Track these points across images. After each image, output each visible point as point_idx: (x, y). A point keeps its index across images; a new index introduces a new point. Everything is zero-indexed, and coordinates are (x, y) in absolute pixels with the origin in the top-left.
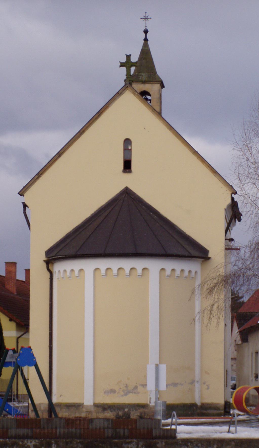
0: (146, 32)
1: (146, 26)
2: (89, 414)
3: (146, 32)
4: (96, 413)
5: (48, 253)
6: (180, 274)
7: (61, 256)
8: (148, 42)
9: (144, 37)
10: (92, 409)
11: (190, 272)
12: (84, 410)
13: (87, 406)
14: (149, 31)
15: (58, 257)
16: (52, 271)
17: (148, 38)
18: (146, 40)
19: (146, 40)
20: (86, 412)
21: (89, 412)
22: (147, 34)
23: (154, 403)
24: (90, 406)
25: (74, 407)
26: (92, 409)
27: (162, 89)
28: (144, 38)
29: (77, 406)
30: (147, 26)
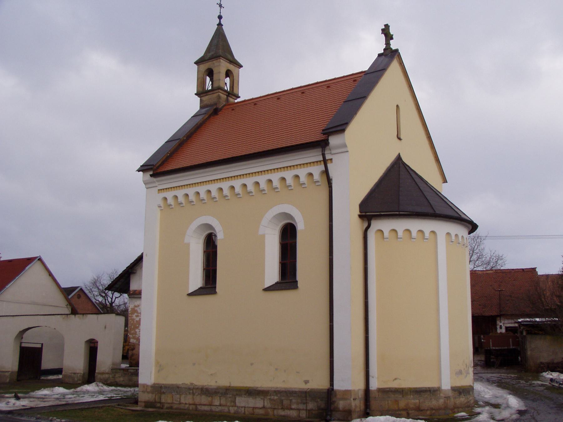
0: (220, 17)
1: (220, 13)
2: (447, 401)
3: (220, 17)
4: (454, 398)
5: (363, 205)
6: (402, 235)
7: (408, 213)
8: (223, 27)
9: (218, 22)
10: (450, 394)
11: (456, 235)
12: (442, 395)
13: (445, 390)
14: (223, 16)
15: (401, 213)
16: (295, 225)
17: (222, 22)
18: (220, 25)
19: (220, 25)
20: (445, 397)
21: (448, 398)
22: (221, 20)
23: (75, 316)
24: (448, 390)
25: (429, 392)
26: (450, 394)
27: (240, 69)
28: (218, 23)
29: (433, 392)
30: (221, 12)
